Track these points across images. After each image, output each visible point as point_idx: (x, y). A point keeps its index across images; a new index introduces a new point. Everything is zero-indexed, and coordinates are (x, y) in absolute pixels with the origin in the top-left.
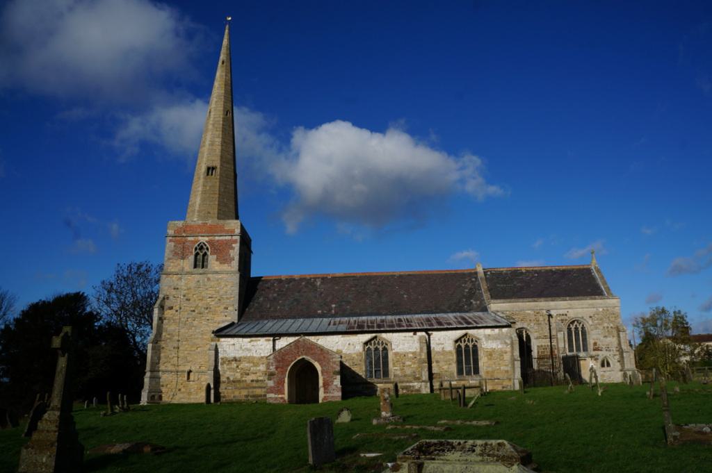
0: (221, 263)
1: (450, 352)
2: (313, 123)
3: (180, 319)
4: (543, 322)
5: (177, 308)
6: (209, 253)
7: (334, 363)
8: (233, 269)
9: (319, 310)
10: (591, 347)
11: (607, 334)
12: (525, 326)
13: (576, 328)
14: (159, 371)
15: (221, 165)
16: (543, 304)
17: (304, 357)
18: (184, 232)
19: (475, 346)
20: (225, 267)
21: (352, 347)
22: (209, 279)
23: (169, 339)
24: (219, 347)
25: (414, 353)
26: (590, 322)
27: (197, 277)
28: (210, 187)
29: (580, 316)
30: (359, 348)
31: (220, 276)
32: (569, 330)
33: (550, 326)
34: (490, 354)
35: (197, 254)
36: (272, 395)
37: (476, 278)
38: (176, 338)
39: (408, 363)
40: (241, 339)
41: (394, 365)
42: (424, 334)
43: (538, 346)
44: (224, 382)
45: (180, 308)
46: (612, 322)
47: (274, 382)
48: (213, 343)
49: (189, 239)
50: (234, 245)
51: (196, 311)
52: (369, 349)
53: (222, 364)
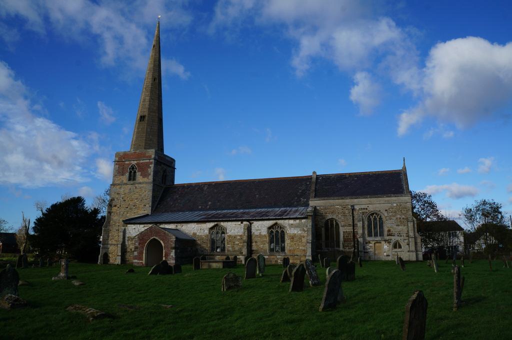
0: (143, 177)
1: (265, 236)
2: (447, 36)
3: (120, 212)
4: (348, 215)
5: (119, 206)
6: (137, 171)
7: (171, 241)
8: (150, 181)
9: (200, 205)
10: (386, 233)
11: (399, 224)
12: (334, 217)
13: (375, 219)
14: (108, 244)
15: (148, 114)
16: (349, 201)
17: (155, 237)
18: (124, 158)
19: (283, 232)
20: (145, 180)
21: (202, 231)
22: (136, 188)
23: (114, 224)
24: (127, 230)
25: (241, 236)
26: (386, 215)
27: (130, 186)
28: (141, 129)
29: (378, 210)
30: (207, 232)
31: (142, 186)
32: (369, 220)
33: (353, 217)
34: (292, 238)
35: (131, 172)
36: (136, 261)
37: (310, 182)
38: (117, 224)
39: (237, 243)
40: (138, 225)
41: (228, 244)
42: (248, 223)
43: (344, 232)
44: (129, 252)
45: (120, 206)
46: (404, 214)
47: (138, 253)
48: (124, 228)
49: (126, 162)
50: (150, 166)
51: (129, 207)
52: (272, 232)
53: (128, 241)
